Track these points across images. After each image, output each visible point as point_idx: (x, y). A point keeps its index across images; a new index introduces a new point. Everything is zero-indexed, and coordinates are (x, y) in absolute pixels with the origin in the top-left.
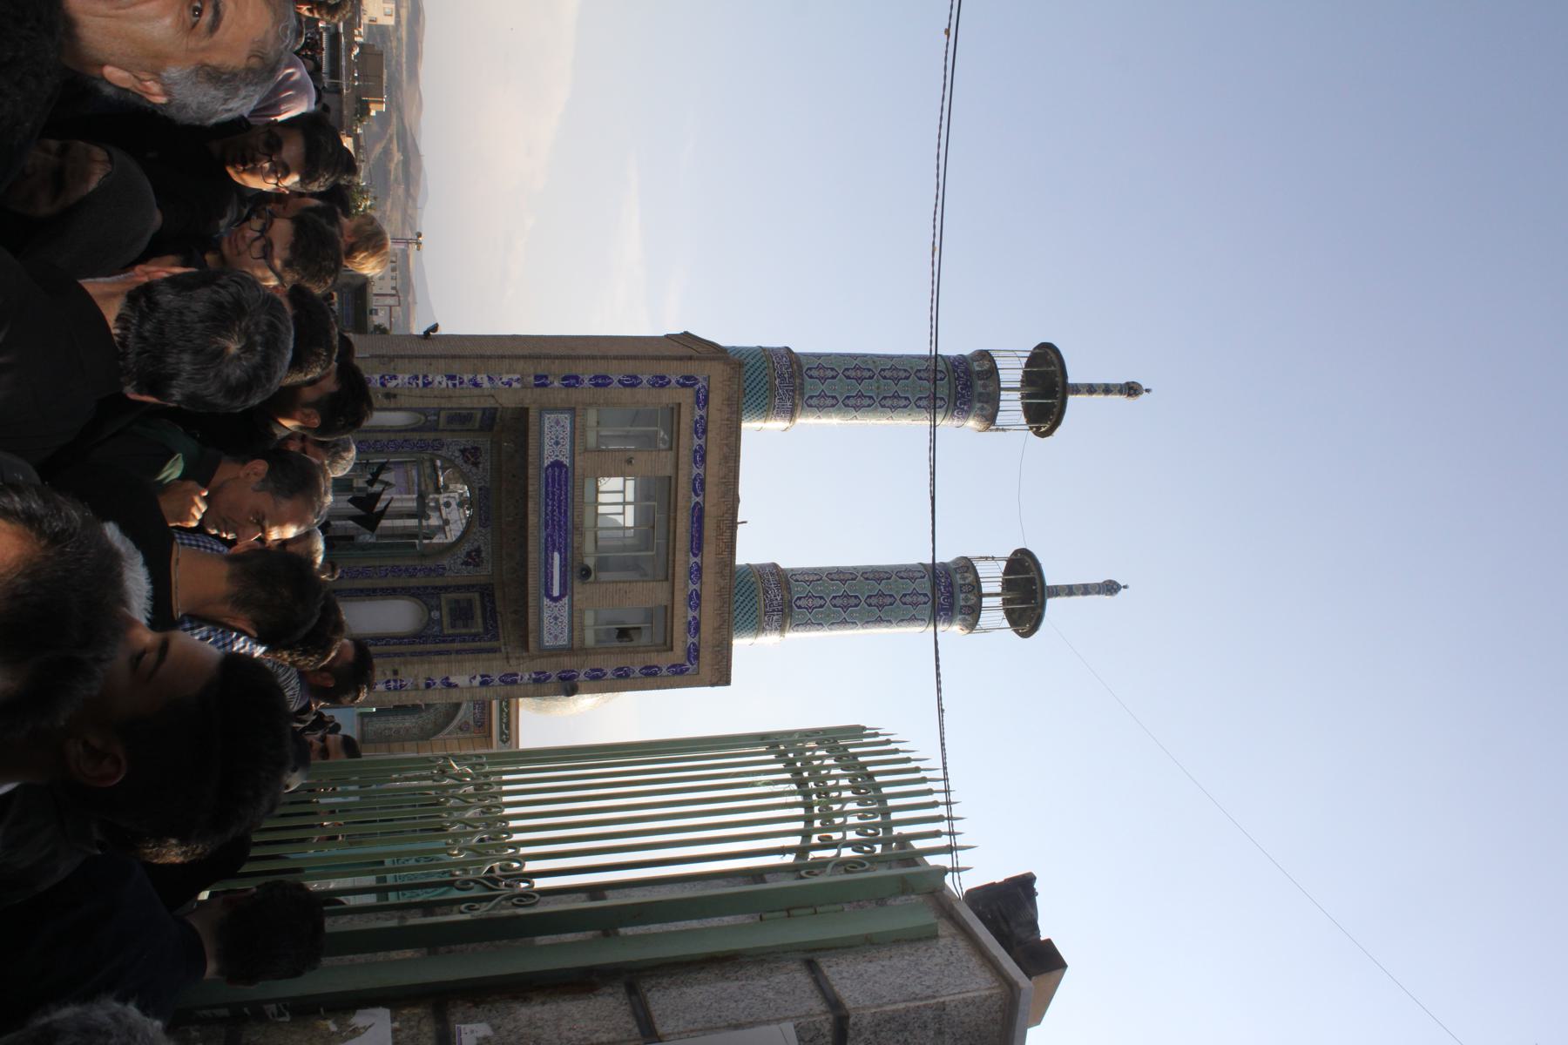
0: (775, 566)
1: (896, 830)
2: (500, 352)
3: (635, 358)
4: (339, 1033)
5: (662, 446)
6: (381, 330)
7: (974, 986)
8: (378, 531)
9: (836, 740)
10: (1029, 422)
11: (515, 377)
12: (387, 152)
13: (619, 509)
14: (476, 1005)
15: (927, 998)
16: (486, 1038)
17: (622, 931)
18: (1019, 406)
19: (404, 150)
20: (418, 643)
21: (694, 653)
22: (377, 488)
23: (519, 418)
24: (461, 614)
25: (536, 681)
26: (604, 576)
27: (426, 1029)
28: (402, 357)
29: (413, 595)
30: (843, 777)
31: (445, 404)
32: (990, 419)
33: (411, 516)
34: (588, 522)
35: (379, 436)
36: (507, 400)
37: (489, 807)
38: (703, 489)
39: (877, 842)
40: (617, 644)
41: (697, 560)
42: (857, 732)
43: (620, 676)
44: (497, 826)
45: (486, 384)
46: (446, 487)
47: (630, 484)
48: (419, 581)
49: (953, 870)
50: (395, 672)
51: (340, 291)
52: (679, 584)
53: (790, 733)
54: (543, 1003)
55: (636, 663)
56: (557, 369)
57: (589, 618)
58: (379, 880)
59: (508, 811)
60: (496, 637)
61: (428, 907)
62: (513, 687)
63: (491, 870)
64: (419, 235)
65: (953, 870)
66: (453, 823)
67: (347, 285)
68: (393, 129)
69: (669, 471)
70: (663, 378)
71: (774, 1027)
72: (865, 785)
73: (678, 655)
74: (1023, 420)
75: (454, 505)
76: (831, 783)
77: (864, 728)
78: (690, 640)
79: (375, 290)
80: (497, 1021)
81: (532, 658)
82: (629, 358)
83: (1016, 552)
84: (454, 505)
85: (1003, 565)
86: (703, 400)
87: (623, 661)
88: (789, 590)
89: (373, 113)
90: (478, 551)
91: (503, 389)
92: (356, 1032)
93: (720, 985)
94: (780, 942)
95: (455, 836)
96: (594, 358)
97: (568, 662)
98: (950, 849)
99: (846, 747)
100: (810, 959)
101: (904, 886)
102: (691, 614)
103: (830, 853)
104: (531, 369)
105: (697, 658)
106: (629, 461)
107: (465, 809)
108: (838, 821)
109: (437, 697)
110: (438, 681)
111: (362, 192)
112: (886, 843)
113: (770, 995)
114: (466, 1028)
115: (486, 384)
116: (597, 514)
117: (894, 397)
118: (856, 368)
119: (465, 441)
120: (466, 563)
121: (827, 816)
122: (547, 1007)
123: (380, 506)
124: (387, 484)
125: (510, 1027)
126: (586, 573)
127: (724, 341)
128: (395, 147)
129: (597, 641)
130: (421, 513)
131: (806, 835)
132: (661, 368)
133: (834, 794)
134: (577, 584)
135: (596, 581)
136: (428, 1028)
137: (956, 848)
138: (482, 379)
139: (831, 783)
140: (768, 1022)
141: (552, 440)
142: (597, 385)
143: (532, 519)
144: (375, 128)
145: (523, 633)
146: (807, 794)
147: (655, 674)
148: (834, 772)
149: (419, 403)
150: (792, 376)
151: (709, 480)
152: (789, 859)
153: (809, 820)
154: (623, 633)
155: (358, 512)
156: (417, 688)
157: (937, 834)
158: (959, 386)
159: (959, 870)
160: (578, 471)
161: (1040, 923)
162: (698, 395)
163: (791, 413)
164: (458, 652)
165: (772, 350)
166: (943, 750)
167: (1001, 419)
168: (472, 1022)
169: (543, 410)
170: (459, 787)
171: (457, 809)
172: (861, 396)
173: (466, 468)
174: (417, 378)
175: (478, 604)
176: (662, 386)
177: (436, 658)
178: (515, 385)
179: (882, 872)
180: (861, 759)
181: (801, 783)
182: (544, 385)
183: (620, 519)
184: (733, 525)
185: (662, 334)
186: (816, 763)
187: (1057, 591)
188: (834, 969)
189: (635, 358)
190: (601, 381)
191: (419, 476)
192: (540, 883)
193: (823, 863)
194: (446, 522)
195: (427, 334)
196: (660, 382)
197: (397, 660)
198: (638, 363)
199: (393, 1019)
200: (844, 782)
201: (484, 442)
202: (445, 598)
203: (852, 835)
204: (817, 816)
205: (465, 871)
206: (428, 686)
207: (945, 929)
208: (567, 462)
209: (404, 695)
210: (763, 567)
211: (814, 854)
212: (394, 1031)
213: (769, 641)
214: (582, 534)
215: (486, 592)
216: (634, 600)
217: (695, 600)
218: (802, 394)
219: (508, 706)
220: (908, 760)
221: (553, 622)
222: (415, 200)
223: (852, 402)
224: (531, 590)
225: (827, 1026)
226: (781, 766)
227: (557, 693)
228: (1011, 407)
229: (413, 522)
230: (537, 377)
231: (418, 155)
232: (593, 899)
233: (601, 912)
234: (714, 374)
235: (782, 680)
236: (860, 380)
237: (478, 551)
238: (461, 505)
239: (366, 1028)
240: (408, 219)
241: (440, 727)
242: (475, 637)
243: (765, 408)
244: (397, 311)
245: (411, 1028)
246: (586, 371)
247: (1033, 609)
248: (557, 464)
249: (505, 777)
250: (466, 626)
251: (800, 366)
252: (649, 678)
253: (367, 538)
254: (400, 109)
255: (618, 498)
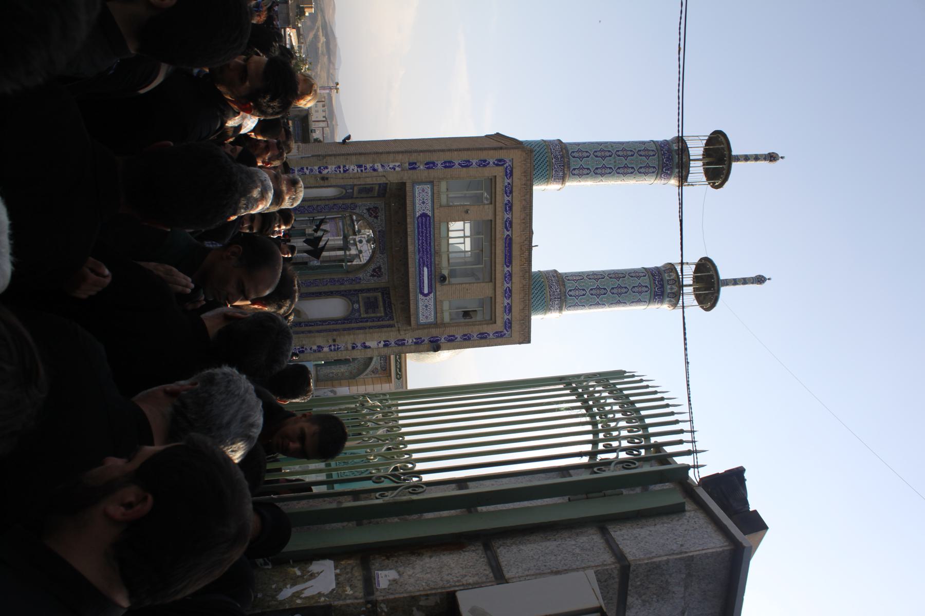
0: (555, 271)
1: (653, 440)
2: (388, 150)
3: (468, 150)
4: (302, 576)
5: (486, 202)
6: (317, 141)
7: (712, 545)
8: (321, 259)
9: (604, 378)
10: (708, 180)
11: (397, 164)
12: (316, 37)
13: (462, 240)
14: (388, 558)
15: (681, 553)
16: (394, 580)
17: (479, 508)
18: (701, 170)
19: (326, 35)
20: (346, 323)
21: (508, 325)
22: (320, 233)
23: (397, 188)
24: (371, 305)
25: (416, 343)
26: (453, 280)
27: (357, 574)
28: (330, 155)
29: (343, 295)
30: (615, 404)
31: (356, 182)
32: (683, 179)
33: (340, 249)
34: (444, 249)
35: (319, 203)
36: (393, 178)
37: (392, 428)
38: (511, 227)
39: (642, 447)
40: (463, 320)
41: (509, 269)
42: (620, 374)
43: (465, 339)
44: (395, 439)
45: (380, 169)
46: (359, 231)
47: (468, 226)
48: (346, 287)
49: (694, 467)
50: (334, 341)
51: (293, 120)
52: (498, 284)
53: (579, 376)
54: (431, 557)
55: (475, 331)
56: (422, 158)
57: (446, 306)
58: (328, 476)
59: (404, 430)
60: (392, 318)
61: (356, 495)
62: (402, 347)
63: (396, 469)
64: (337, 84)
65: (694, 467)
66: (370, 438)
67: (297, 116)
68: (319, 23)
69: (490, 217)
70: (485, 161)
71: (581, 573)
72: (630, 410)
73: (499, 325)
74: (704, 179)
75: (364, 242)
76: (607, 408)
77: (625, 372)
78: (506, 317)
79: (314, 118)
80: (401, 569)
81: (413, 330)
82: (464, 150)
83: (701, 260)
84: (364, 242)
85: (693, 267)
86: (509, 174)
87: (466, 330)
88: (564, 285)
89: (307, 14)
90: (380, 268)
91: (390, 172)
92: (313, 576)
93: (544, 544)
94: (583, 515)
95: (371, 447)
96: (443, 151)
97: (434, 332)
98: (688, 453)
99: (615, 384)
100: (602, 524)
101: (661, 477)
102: (506, 301)
103: (612, 456)
104: (406, 159)
105: (510, 327)
106: (467, 212)
107: (377, 429)
108: (615, 433)
109: (359, 354)
110: (359, 345)
111: (303, 61)
112: (647, 448)
113: (578, 551)
114: (382, 573)
115: (380, 169)
116: (448, 244)
117: (625, 167)
118: (601, 151)
119: (370, 203)
120: (372, 276)
121: (607, 430)
122: (433, 559)
123: (322, 244)
124: (325, 231)
125: (410, 573)
126: (443, 279)
127: (521, 138)
128: (320, 33)
129: (451, 319)
130: (345, 247)
131: (595, 443)
132: (483, 155)
133: (611, 416)
134: (438, 285)
135: (449, 284)
136: (358, 574)
137: (696, 452)
138: (378, 166)
139: (607, 408)
140: (577, 570)
141: (420, 201)
142: (445, 167)
143: (410, 248)
144: (309, 23)
145: (407, 315)
146: (593, 416)
147: (486, 338)
148: (609, 401)
149: (342, 182)
150: (562, 157)
151: (514, 221)
152: (585, 460)
153: (595, 433)
154: (466, 314)
155: (309, 248)
156: (347, 349)
157: (681, 442)
158: (668, 159)
159: (698, 467)
160: (437, 219)
161: (749, 499)
162: (504, 172)
163: (563, 179)
164: (370, 327)
165: (550, 141)
166: (688, 389)
167: (691, 178)
168: (385, 569)
169: (414, 183)
170: (373, 414)
171: (372, 429)
172: (604, 167)
173: (371, 219)
174: (339, 167)
175: (380, 299)
176: (485, 166)
177: (358, 331)
178: (397, 169)
179: (647, 468)
180: (625, 392)
181: (589, 408)
182: (414, 168)
183: (462, 247)
184: (530, 248)
185: (483, 135)
186: (597, 395)
187: (727, 283)
188: (618, 533)
189: (468, 150)
190: (448, 165)
191: (343, 225)
192: (426, 478)
193: (607, 463)
194: (360, 252)
195: (344, 141)
196: (483, 163)
197: (335, 333)
198: (469, 152)
199: (336, 568)
200: (616, 408)
201: (380, 204)
202: (361, 296)
203: (625, 443)
204: (601, 431)
205: (379, 470)
206: (353, 348)
207: (689, 506)
208: (430, 214)
209: (339, 354)
210: (548, 272)
211: (600, 457)
212: (337, 575)
213: (553, 317)
214: (440, 256)
215: (385, 292)
216: (471, 294)
217: (508, 293)
218: (569, 168)
219: (400, 358)
220: (656, 392)
221: (424, 309)
222: (334, 64)
223: (599, 171)
224: (411, 290)
225: (616, 572)
226: (574, 398)
227: (428, 350)
228: (697, 171)
229: (341, 253)
230: (410, 164)
231: (335, 38)
232: (461, 488)
233: (467, 497)
234: (516, 157)
235: (563, 342)
236: (604, 157)
237: (380, 268)
238: (368, 241)
239: (319, 574)
240: (330, 75)
241: (360, 372)
242: (379, 319)
243: (547, 177)
244: (327, 130)
245: (347, 573)
246: (439, 159)
247: (712, 294)
248: (424, 215)
249: (400, 408)
250: (374, 312)
251: (567, 151)
252: (483, 340)
253: (315, 263)
254: (322, 11)
255: (461, 234)
